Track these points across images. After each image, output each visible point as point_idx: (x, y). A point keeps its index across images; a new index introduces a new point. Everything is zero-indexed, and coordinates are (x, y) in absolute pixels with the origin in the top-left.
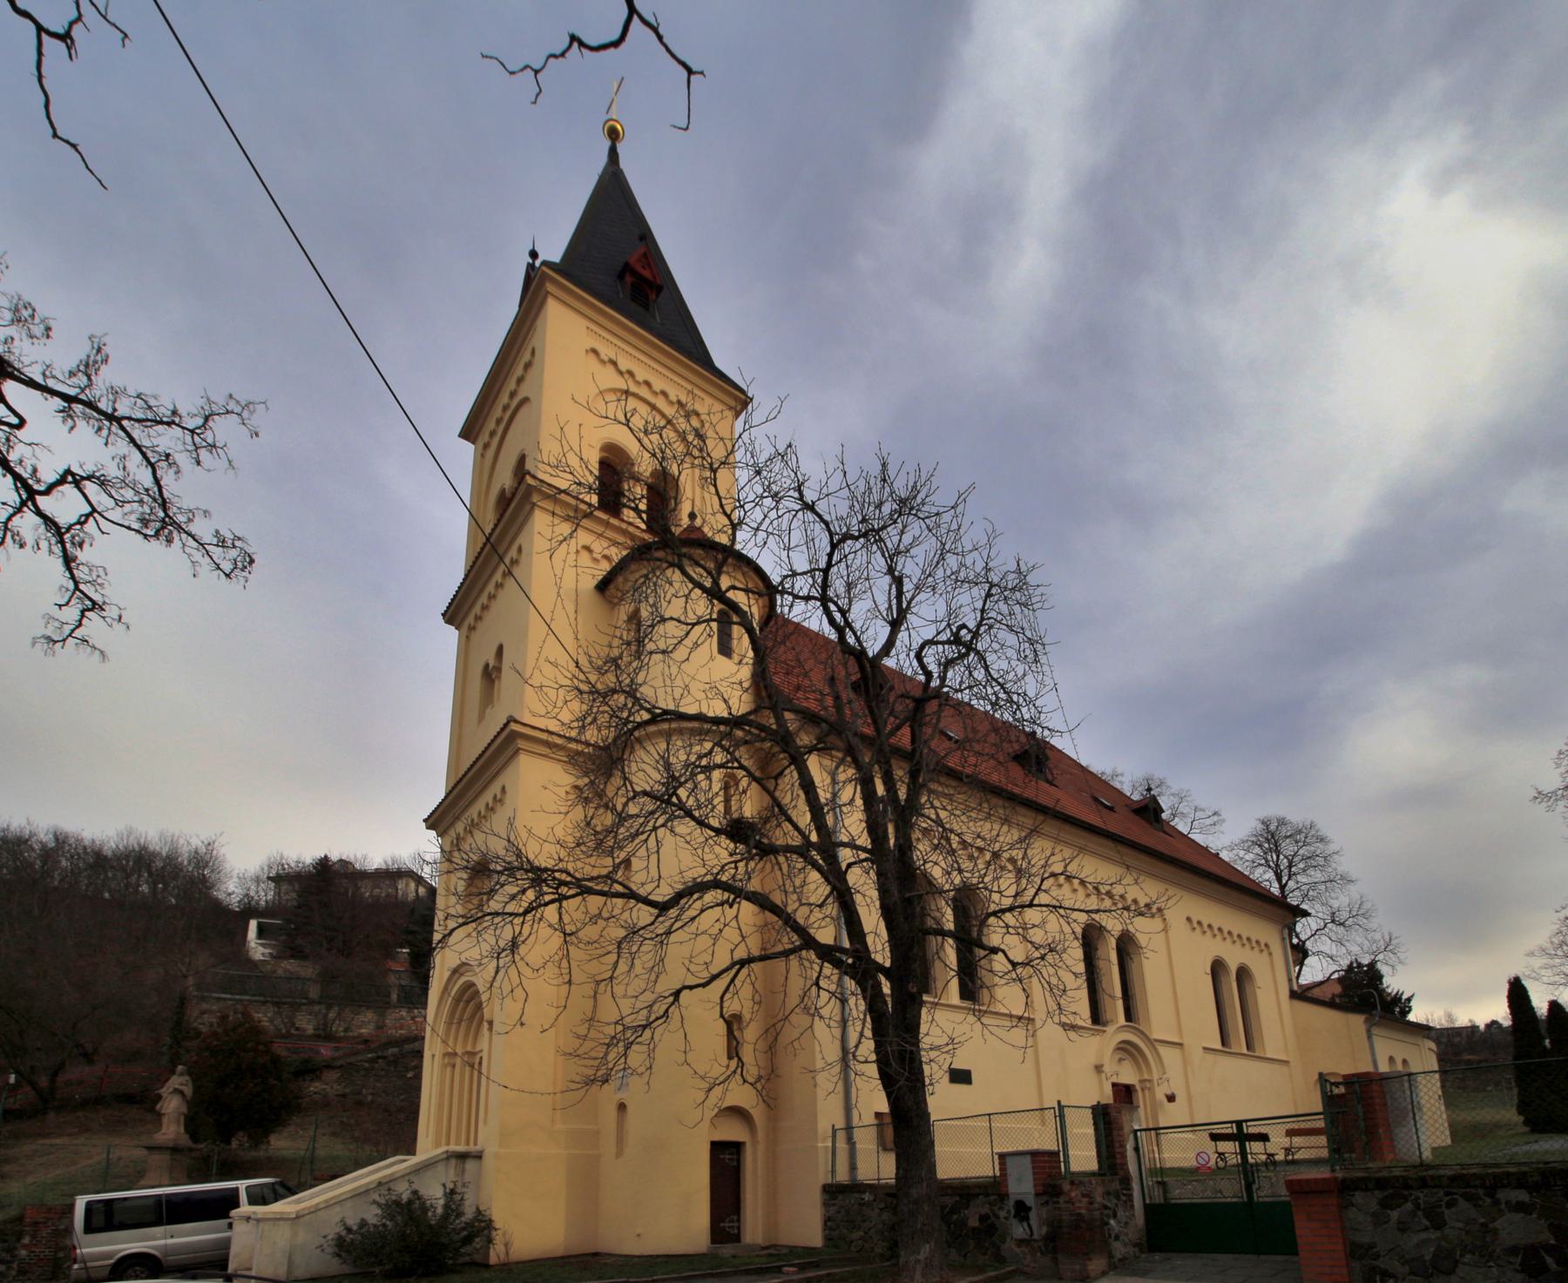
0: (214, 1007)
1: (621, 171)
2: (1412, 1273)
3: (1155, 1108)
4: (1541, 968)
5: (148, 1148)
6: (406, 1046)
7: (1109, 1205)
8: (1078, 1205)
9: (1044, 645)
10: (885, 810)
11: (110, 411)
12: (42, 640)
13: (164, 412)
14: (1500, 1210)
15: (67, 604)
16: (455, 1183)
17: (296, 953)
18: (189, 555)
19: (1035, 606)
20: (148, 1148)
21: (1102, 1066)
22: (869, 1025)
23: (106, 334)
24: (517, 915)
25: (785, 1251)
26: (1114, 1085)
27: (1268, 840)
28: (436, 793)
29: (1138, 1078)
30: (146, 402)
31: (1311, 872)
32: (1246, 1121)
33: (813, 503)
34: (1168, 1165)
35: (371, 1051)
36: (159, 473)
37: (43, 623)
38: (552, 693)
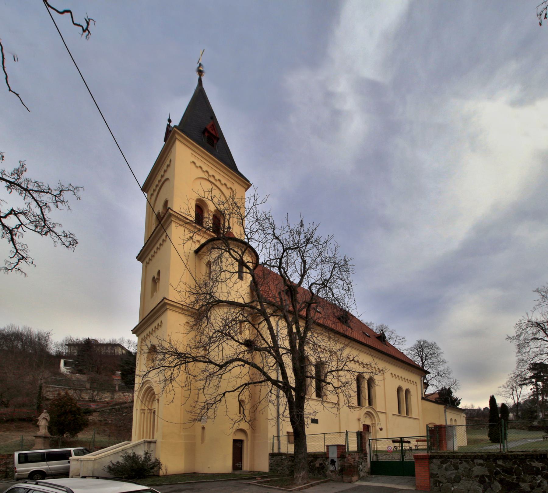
0: (51, 390)
1: (203, 89)
2: (448, 482)
3: (376, 432)
4: (503, 392)
5: (35, 437)
6: (123, 405)
7: (360, 461)
8: (350, 461)
9: (351, 285)
10: (296, 337)
11: (25, 187)
12: (3, 269)
13: (45, 188)
14: (475, 465)
15: (14, 257)
16: (148, 450)
17: (81, 372)
18: (53, 239)
19: (350, 272)
20: (35, 437)
21: (360, 419)
22: (288, 406)
23: (25, 161)
24: (172, 367)
25: (256, 473)
26: (363, 425)
27: (419, 348)
28: (135, 322)
29: (371, 423)
30: (38, 184)
31: (433, 359)
32: (404, 438)
33: (278, 236)
34: (379, 449)
35: (110, 406)
36: (43, 210)
37: (4, 262)
38: (184, 294)
